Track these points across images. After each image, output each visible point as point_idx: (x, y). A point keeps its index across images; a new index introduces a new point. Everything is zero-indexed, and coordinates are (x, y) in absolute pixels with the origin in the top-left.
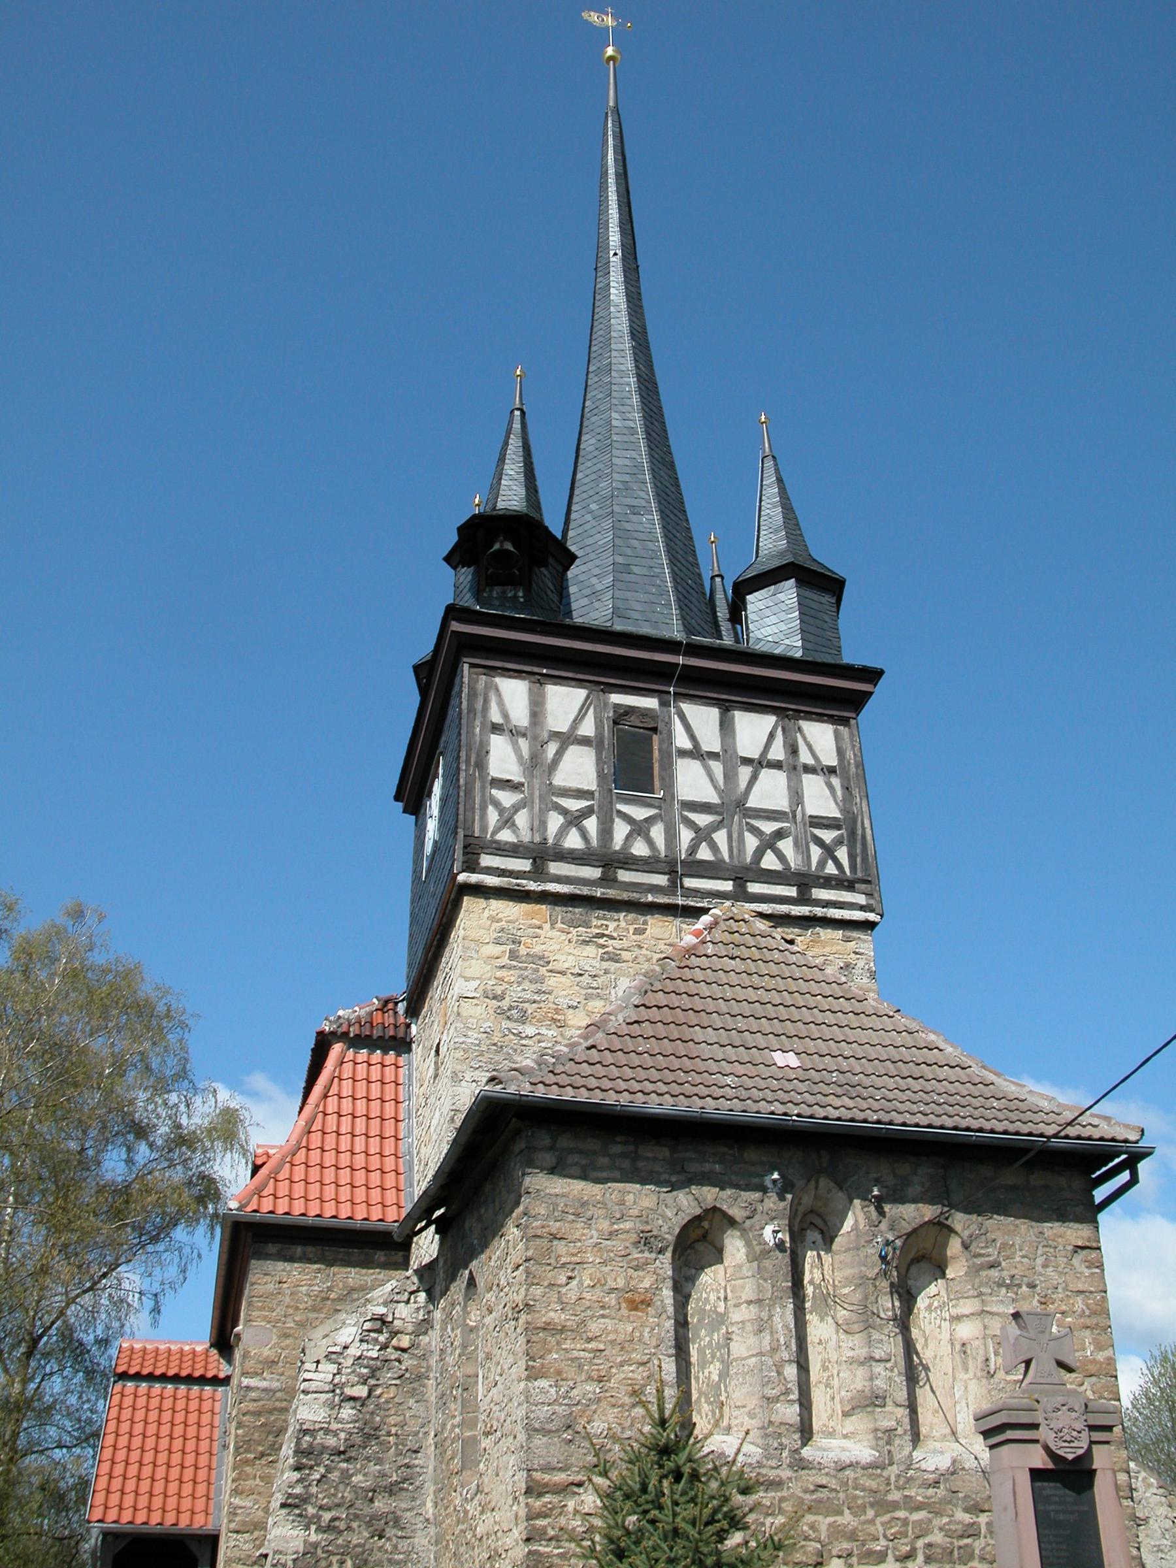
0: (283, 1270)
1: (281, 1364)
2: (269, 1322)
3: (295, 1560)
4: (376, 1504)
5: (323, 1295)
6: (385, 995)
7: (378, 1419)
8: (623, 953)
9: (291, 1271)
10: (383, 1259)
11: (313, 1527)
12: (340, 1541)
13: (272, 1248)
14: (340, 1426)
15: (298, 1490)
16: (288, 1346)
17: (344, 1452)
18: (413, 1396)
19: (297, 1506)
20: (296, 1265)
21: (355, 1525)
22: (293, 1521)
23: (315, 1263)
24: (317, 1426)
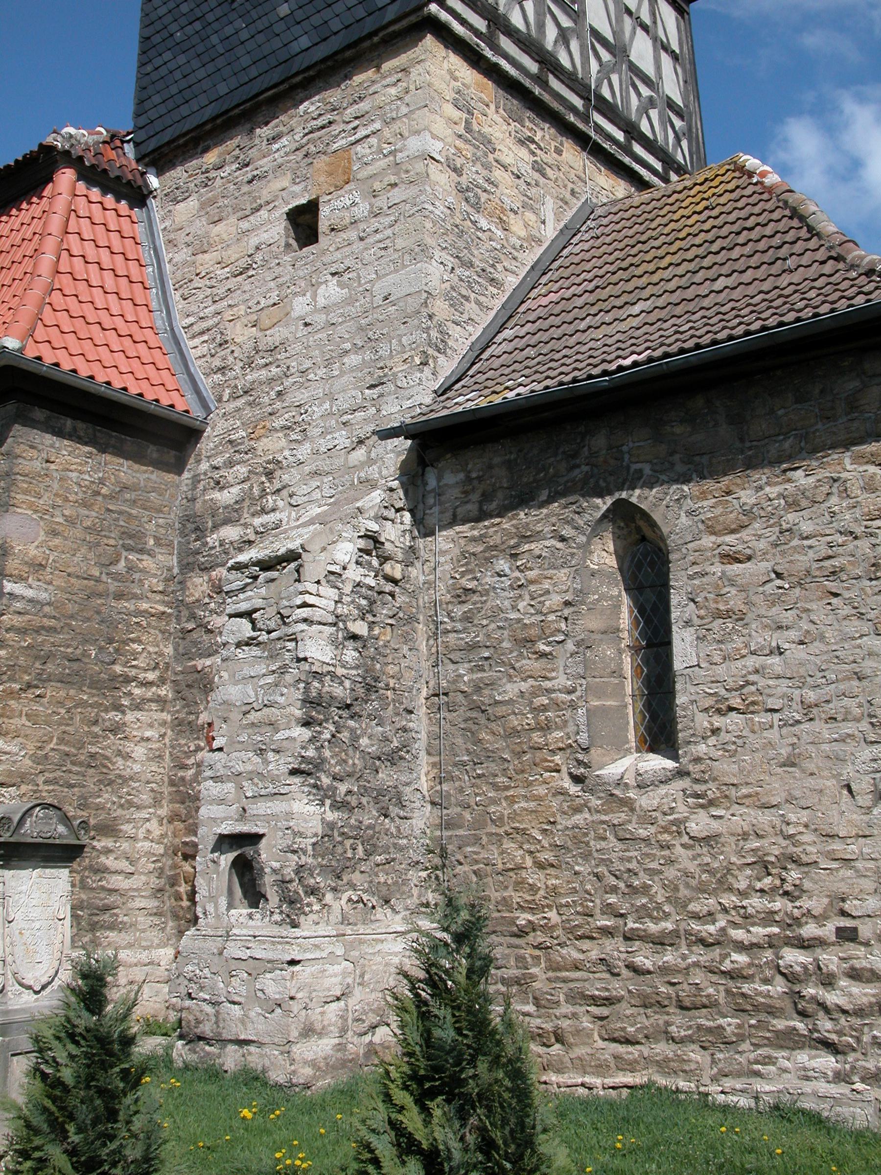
0: (52, 446)
1: (48, 570)
2: (36, 511)
3: (314, 844)
4: (380, 775)
5: (94, 486)
6: (115, 128)
7: (378, 666)
8: (548, 169)
9: (59, 449)
10: (155, 455)
11: (328, 802)
12: (352, 821)
13: (39, 414)
14: (344, 671)
15: (311, 753)
16: (56, 546)
17: (348, 706)
18: (405, 643)
19: (309, 774)
20: (66, 442)
21: (364, 800)
22: (310, 793)
23: (86, 444)
24: (326, 669)
